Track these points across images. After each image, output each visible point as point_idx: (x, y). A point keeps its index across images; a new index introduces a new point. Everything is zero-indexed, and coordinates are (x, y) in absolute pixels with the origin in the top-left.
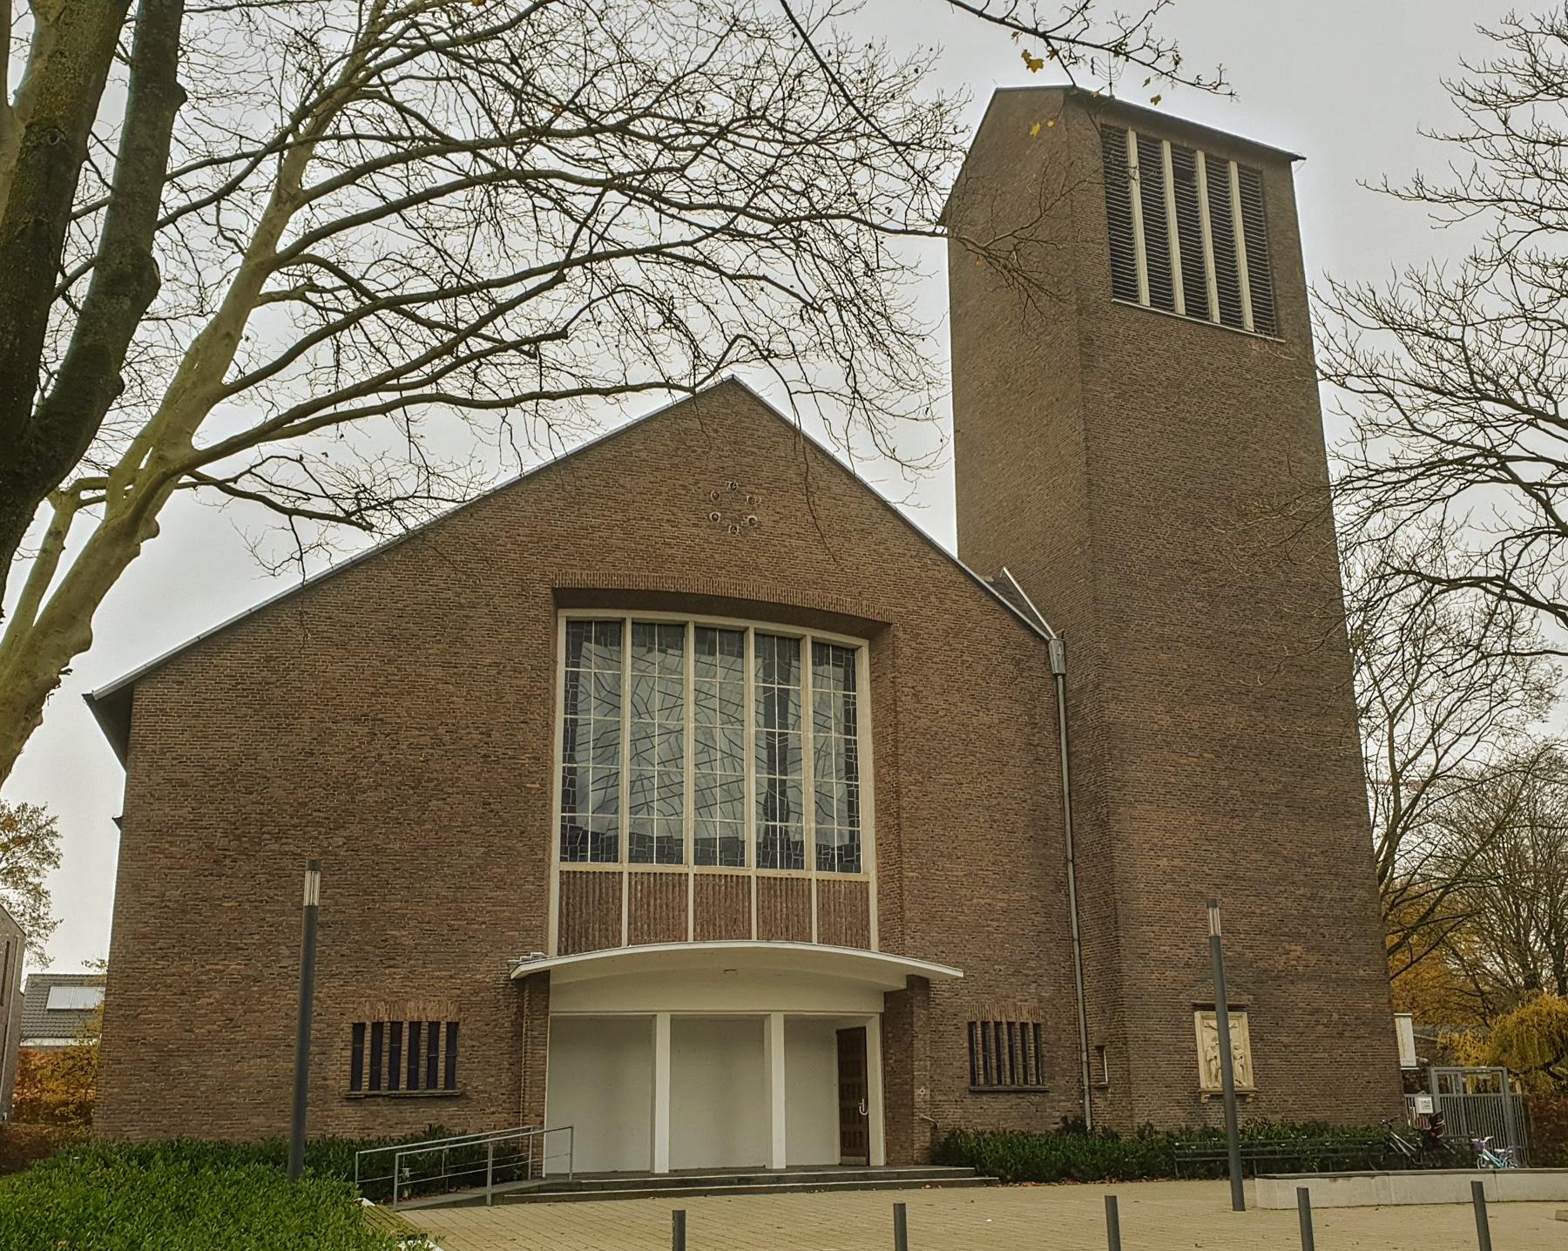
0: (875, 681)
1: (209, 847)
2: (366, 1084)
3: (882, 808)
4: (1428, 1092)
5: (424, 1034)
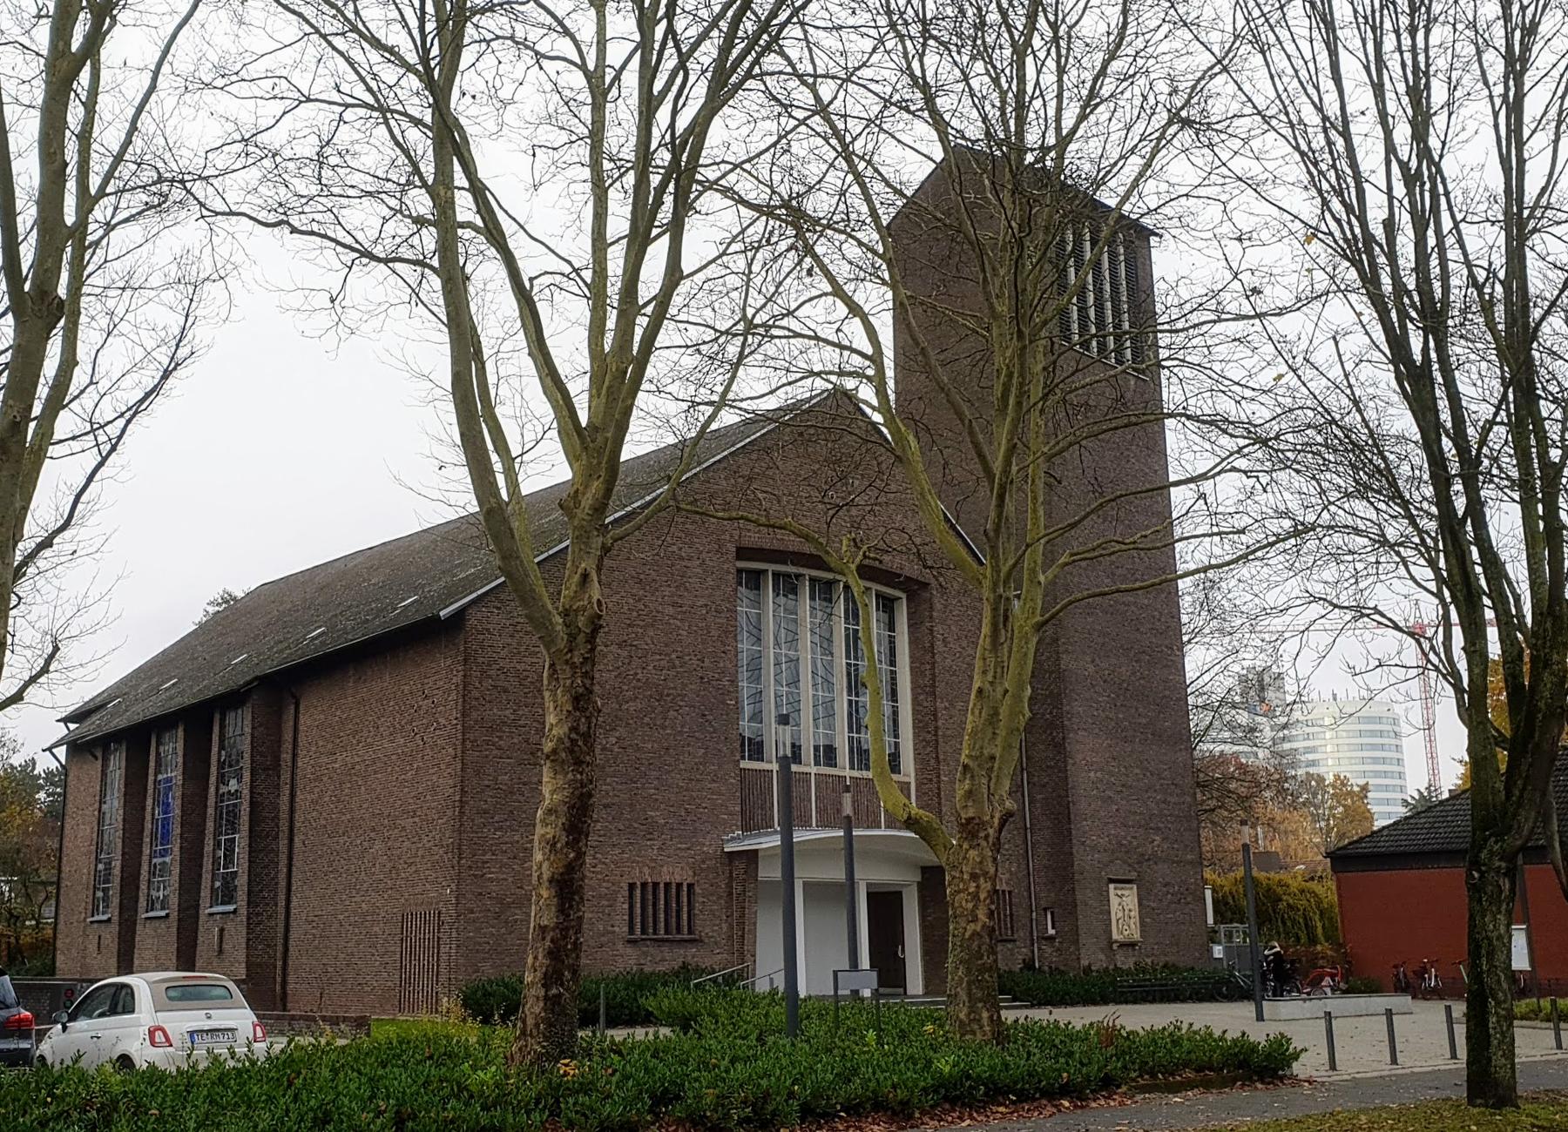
0: (912, 626)
1: (526, 741)
2: (638, 931)
3: (919, 726)
4: (1219, 943)
5: (650, 889)
